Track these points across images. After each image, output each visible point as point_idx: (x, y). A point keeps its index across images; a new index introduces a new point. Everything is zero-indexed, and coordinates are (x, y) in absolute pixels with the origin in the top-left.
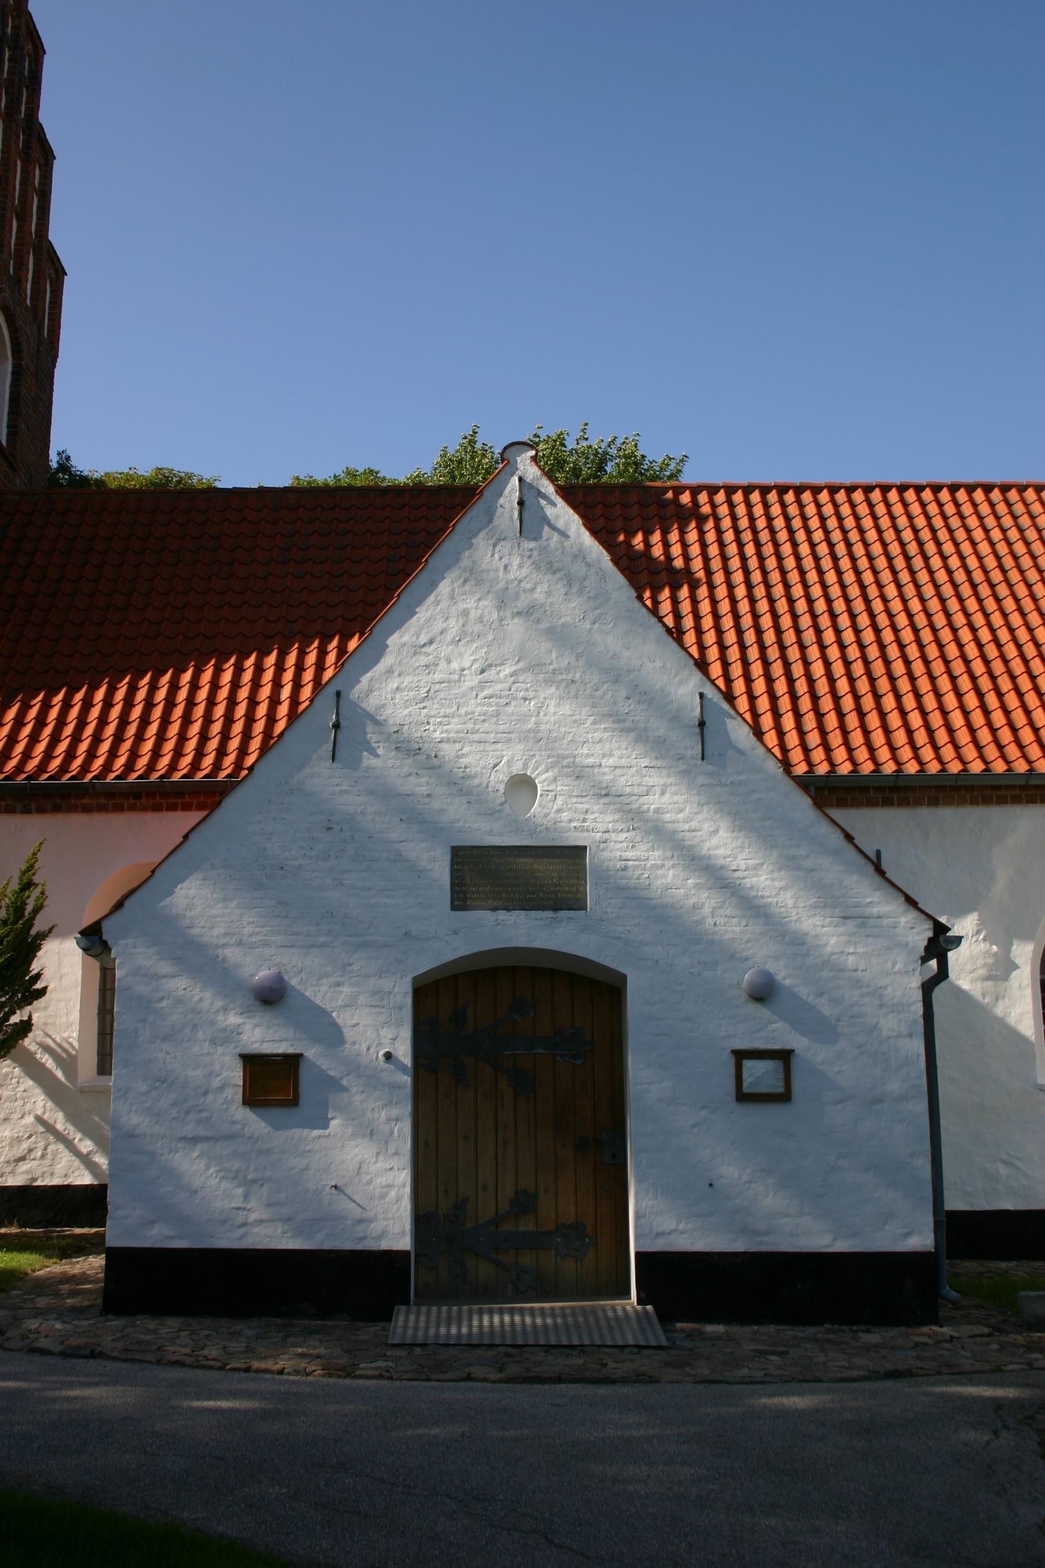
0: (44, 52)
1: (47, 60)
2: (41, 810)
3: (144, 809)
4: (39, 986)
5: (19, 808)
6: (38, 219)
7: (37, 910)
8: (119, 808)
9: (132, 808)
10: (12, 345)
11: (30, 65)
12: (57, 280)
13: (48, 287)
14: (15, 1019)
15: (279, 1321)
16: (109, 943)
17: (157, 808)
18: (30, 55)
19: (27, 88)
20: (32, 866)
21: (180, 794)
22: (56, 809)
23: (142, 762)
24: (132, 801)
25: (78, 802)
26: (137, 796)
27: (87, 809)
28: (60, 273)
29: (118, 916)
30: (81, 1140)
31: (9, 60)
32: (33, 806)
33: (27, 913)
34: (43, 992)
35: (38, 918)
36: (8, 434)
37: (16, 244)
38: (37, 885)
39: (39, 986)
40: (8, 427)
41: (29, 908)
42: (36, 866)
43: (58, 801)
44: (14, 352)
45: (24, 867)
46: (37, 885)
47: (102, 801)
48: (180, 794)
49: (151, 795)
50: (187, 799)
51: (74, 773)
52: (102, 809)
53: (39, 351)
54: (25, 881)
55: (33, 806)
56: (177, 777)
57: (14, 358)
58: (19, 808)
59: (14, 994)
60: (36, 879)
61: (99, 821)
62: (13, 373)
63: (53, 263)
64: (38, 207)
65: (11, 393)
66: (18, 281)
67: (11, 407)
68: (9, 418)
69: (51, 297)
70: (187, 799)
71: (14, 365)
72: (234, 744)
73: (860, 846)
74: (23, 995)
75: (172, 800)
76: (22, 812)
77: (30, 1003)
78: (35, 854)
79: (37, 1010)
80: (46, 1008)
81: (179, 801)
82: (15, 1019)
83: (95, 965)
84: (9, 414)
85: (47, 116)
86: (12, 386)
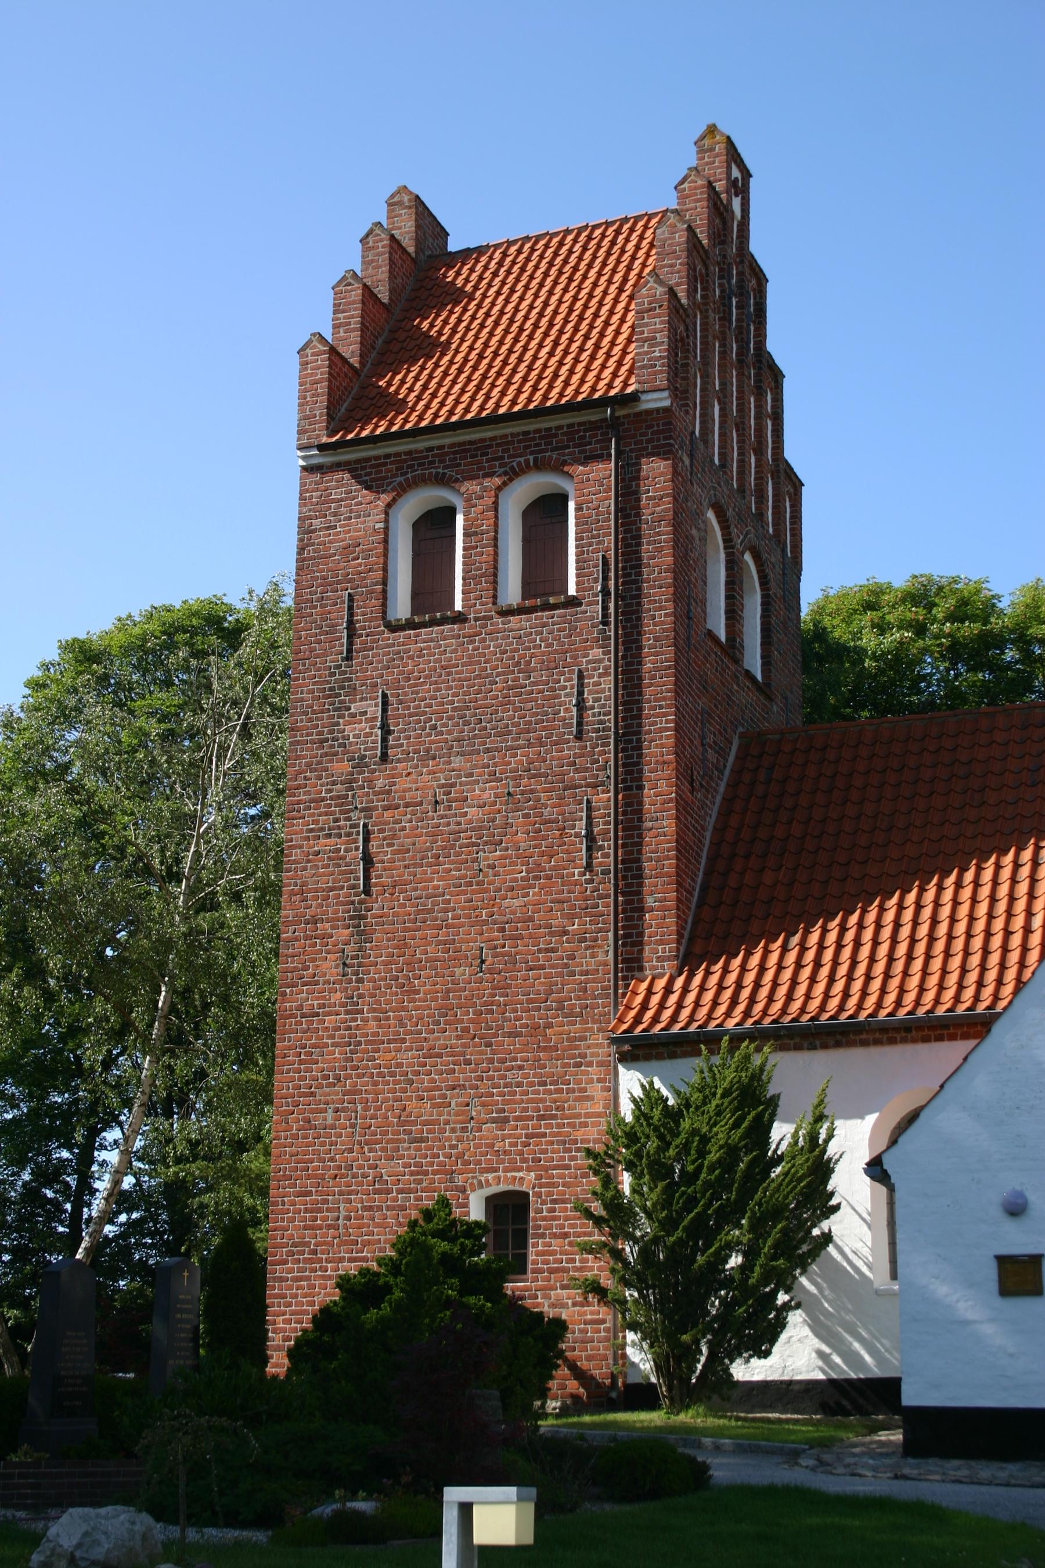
0: (767, 281)
1: (770, 288)
2: (825, 1046)
3: (914, 1041)
4: (833, 1202)
5: (806, 1045)
6: (773, 442)
7: (827, 1141)
8: (892, 1041)
9: (904, 1041)
10: (760, 578)
11: (755, 298)
12: (796, 494)
13: (788, 504)
14: (816, 1232)
15: (1038, 1464)
16: (889, 1172)
17: (926, 1040)
18: (754, 290)
19: (754, 322)
20: (822, 1101)
21: (946, 1027)
22: (838, 1045)
23: (910, 998)
24: (904, 1034)
25: (857, 1038)
26: (908, 1030)
27: (865, 1043)
28: (797, 485)
29: (894, 1150)
30: (555, 1398)
31: (737, 308)
32: (818, 1043)
33: (820, 1142)
34: (836, 1208)
35: (831, 1144)
36: (763, 664)
37: (755, 479)
38: (827, 1117)
39: (833, 1202)
40: (762, 657)
41: (823, 1136)
42: (826, 1100)
43: (839, 1037)
44: (761, 584)
45: (816, 1101)
46: (827, 1117)
47: (877, 1035)
48: (946, 1027)
49: (919, 1028)
50: (952, 1030)
51: (851, 1012)
52: (878, 1042)
53: (784, 574)
54: (817, 1113)
55: (818, 1043)
56: (941, 1011)
57: (762, 590)
58: (806, 1045)
59: (815, 1211)
60: (826, 1112)
61: (875, 1052)
62: (762, 604)
63: (791, 480)
64: (773, 431)
65: (762, 624)
66: (761, 515)
67: (763, 637)
68: (762, 649)
69: (791, 512)
70: (952, 1030)
71: (763, 596)
72: (991, 975)
73: (493, 1500)
74: (822, 1211)
75: (939, 1032)
76: (809, 1049)
77: (828, 1218)
78: (824, 1090)
79: (835, 1223)
80: (841, 1221)
81: (945, 1032)
82: (816, 1232)
83: (883, 1190)
84: (762, 644)
85: (774, 345)
86: (762, 617)
